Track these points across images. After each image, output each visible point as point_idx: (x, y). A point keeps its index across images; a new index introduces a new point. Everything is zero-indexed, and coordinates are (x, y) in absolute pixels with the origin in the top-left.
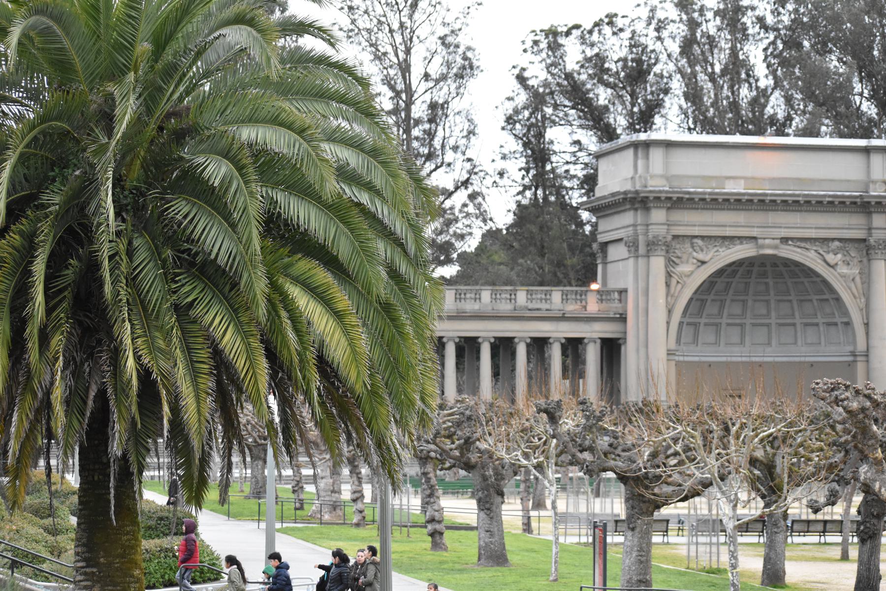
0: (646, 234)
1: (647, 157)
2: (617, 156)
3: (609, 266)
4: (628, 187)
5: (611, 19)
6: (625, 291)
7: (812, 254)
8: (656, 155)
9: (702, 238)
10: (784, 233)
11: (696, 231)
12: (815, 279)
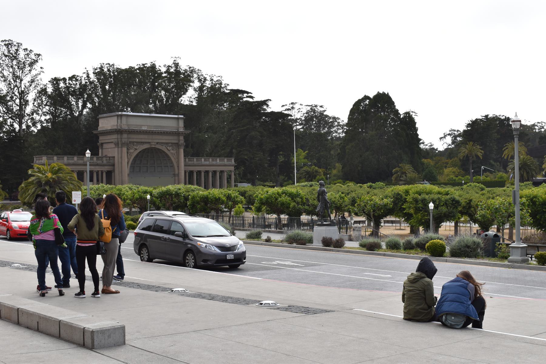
0: (121, 141)
1: (121, 119)
3: (104, 150)
4: (115, 128)
5: (73, 77)
6: (114, 157)
7: (164, 147)
8: (124, 119)
9: (136, 142)
10: (157, 141)
11: (135, 140)
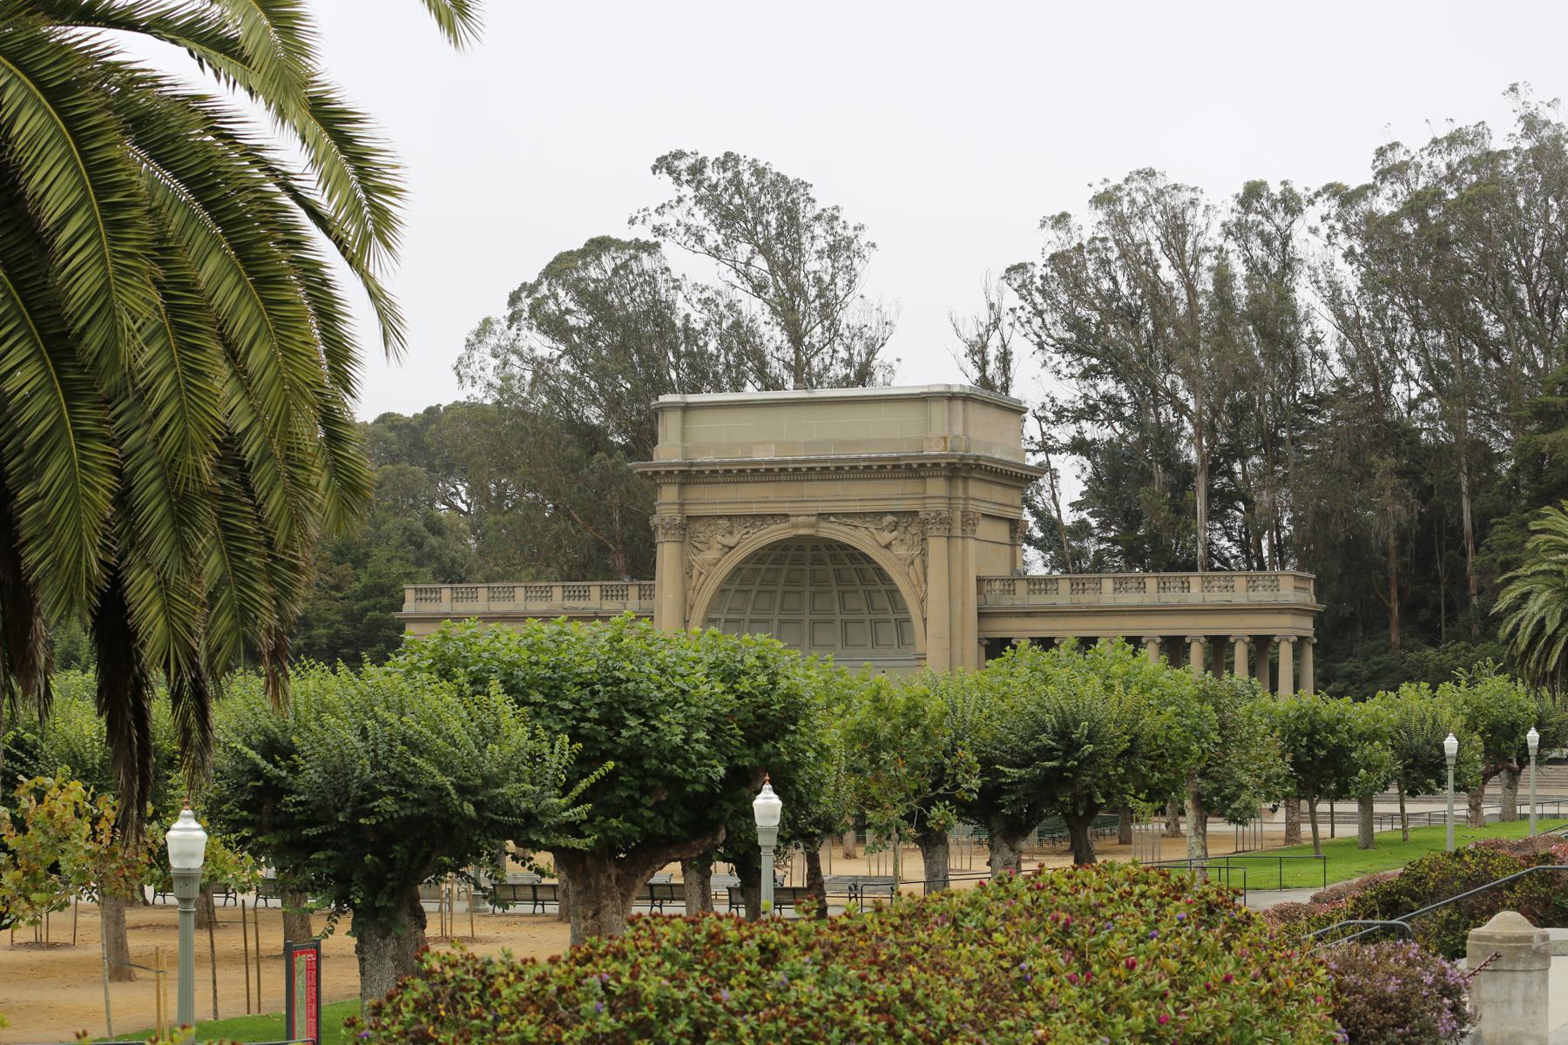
2: (803, 410)
9: (729, 517)
12: (866, 566)
